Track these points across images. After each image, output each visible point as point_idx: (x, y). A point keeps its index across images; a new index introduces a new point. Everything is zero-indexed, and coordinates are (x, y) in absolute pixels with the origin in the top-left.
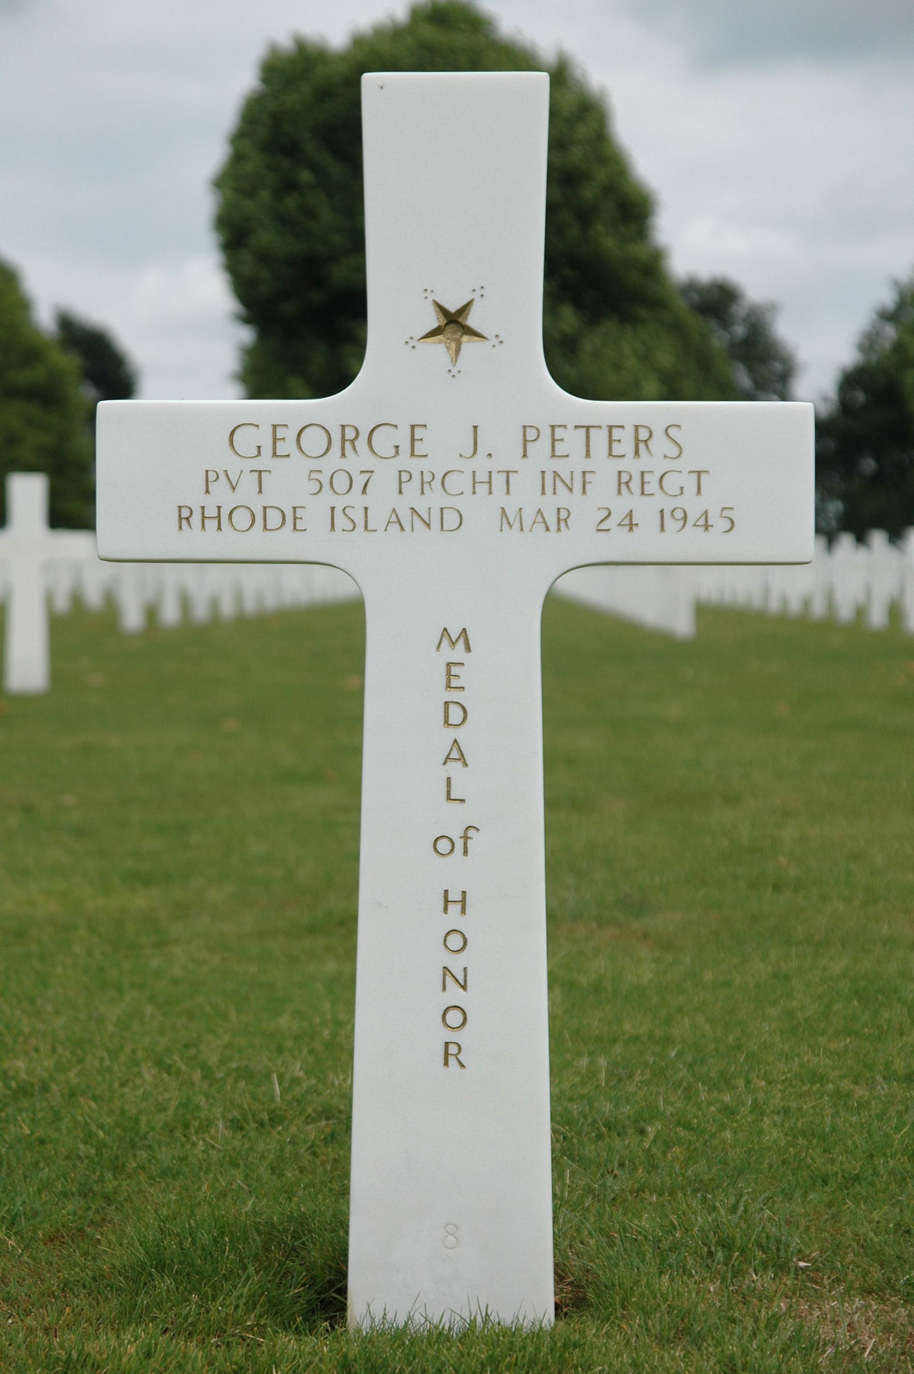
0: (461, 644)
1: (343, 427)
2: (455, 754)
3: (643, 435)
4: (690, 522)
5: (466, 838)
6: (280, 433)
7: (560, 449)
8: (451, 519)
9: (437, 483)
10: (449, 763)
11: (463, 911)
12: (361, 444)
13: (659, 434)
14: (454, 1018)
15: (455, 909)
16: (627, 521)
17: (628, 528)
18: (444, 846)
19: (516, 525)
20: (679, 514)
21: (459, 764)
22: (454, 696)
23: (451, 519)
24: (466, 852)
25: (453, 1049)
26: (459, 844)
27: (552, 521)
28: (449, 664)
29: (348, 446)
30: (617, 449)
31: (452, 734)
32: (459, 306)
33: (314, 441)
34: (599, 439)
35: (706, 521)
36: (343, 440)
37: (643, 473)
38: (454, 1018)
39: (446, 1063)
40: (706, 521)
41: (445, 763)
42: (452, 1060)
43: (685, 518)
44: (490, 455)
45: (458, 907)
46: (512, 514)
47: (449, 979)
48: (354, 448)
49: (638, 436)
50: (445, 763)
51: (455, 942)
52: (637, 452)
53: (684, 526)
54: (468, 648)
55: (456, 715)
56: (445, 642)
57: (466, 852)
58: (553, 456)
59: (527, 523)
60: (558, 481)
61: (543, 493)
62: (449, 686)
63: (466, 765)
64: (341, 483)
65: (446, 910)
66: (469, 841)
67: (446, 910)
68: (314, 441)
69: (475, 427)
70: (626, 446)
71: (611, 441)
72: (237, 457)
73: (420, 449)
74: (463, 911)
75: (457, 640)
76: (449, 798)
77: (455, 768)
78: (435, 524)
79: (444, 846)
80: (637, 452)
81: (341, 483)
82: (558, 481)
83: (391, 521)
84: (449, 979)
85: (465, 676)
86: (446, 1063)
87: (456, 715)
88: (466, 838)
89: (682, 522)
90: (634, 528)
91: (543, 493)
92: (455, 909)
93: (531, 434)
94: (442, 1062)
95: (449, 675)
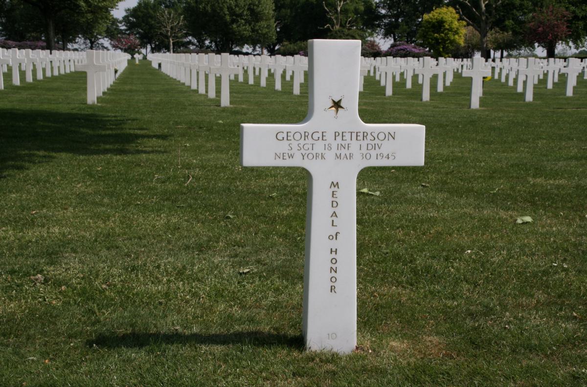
0: (337, 186)
1: (305, 132)
2: (334, 215)
3: (365, 134)
4: (384, 157)
5: (336, 235)
6: (289, 134)
7: (344, 138)
8: (368, 156)
9: (310, 136)
11: (336, 254)
12: (310, 136)
13: (369, 134)
18: (331, 237)
19: (339, 158)
21: (335, 217)
22: (334, 199)
23: (368, 156)
24: (336, 239)
25: (333, 288)
27: (348, 157)
28: (333, 192)
30: (359, 138)
34: (354, 135)
36: (305, 136)
37: (343, 133)
38: (333, 280)
39: (331, 291)
41: (331, 217)
42: (333, 291)
46: (338, 155)
47: (332, 270)
49: (45, 74)
51: (334, 261)
52: (363, 139)
54: (338, 188)
55: (335, 204)
56: (333, 186)
57: (336, 239)
59: (342, 158)
62: (333, 196)
65: (336, 249)
67: (336, 249)
68: (297, 136)
70: (361, 138)
71: (357, 136)
73: (324, 138)
74: (336, 254)
76: (333, 225)
77: (334, 218)
78: (281, 157)
79: (331, 237)
80: (363, 139)
84: (332, 270)
85: (337, 194)
86: (331, 291)
87: (335, 204)
88: (336, 235)
93: (337, 134)
94: (330, 291)
95: (333, 194)
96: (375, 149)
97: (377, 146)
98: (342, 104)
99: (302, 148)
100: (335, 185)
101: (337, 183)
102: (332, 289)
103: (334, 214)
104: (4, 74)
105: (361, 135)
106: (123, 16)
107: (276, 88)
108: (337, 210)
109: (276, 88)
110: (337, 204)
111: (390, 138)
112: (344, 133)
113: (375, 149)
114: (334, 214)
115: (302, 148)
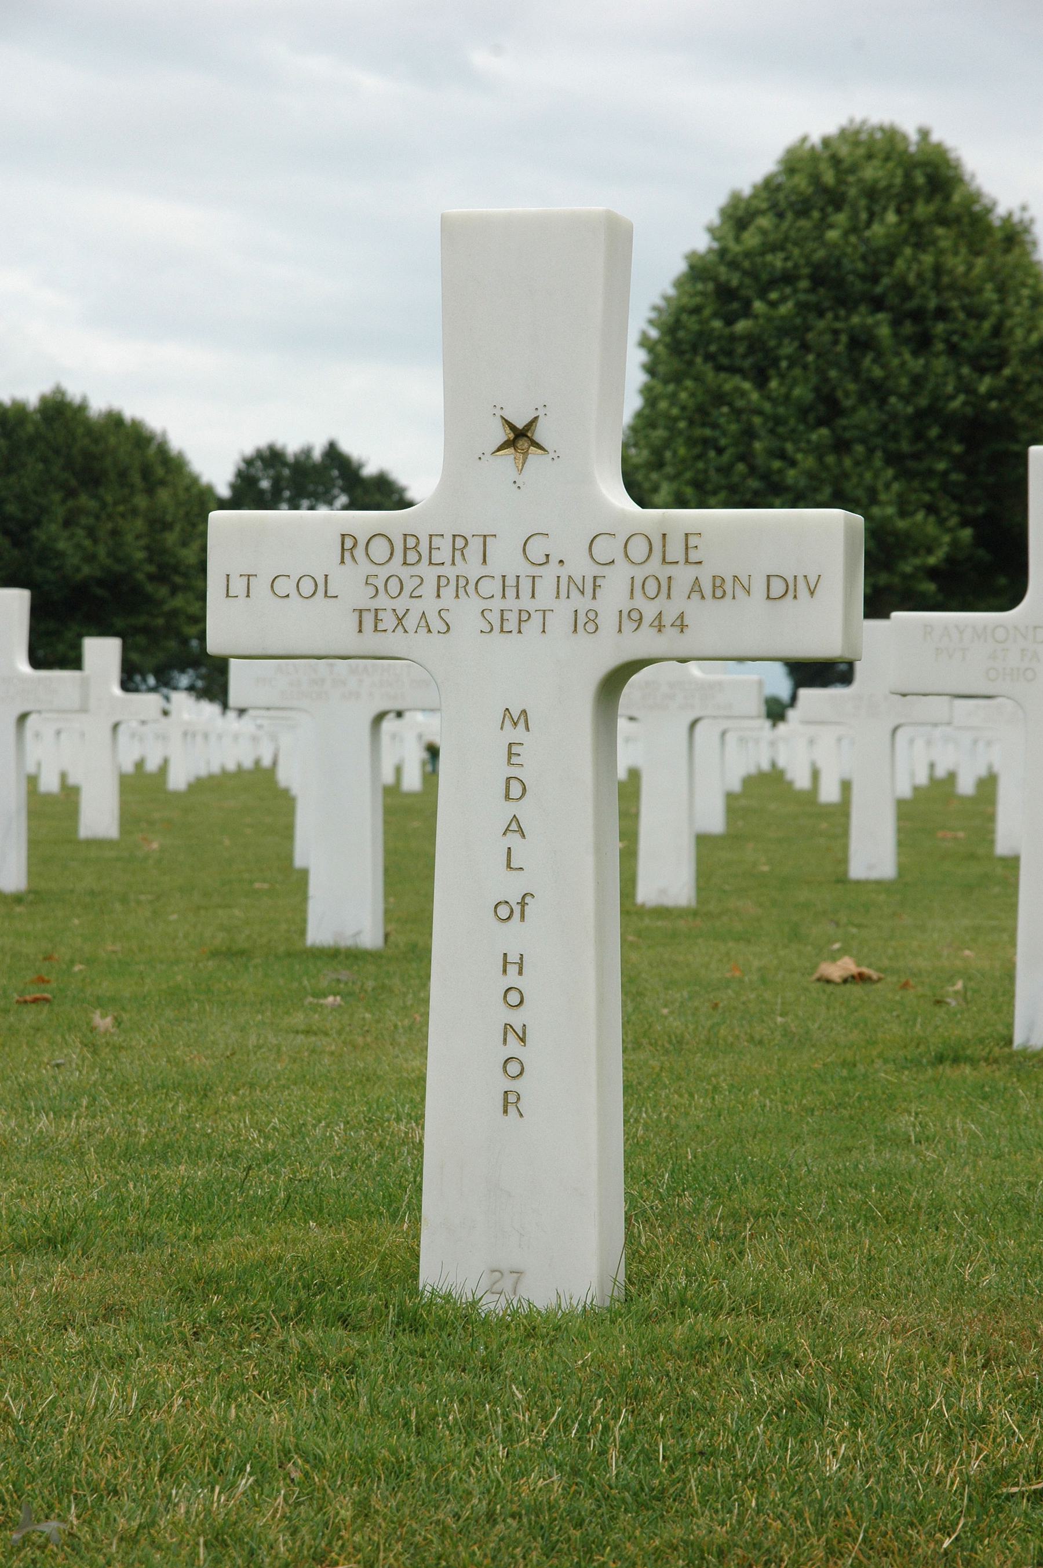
2: (514, 826)
5: (523, 904)
9: (471, 588)
10: (509, 834)
11: (520, 973)
12: (359, 552)
14: (513, 1068)
15: (512, 969)
16: (678, 623)
17: (656, 629)
20: (635, 615)
21: (518, 835)
25: (512, 1098)
26: (517, 910)
29: (458, 554)
31: (512, 808)
32: (508, 431)
33: (379, 550)
35: (660, 622)
37: (595, 578)
39: (505, 1112)
40: (660, 622)
42: (511, 1109)
43: (641, 619)
44: (561, 561)
45: (516, 968)
48: (353, 556)
50: (504, 834)
53: (639, 625)
54: (527, 729)
55: (516, 790)
58: (405, 563)
60: (572, 585)
61: (558, 597)
63: (523, 836)
64: (394, 586)
66: (526, 907)
67: (505, 971)
69: (664, 535)
72: (633, 565)
74: (520, 973)
75: (519, 718)
76: (509, 866)
77: (514, 839)
79: (504, 912)
81: (394, 586)
82: (572, 585)
83: (400, 617)
86: (505, 1112)
87: (516, 790)
89: (636, 625)
90: (662, 629)
91: (558, 597)
92: (512, 969)
94: (501, 1109)
95: (510, 754)
96: (669, 596)
97: (801, 581)
98: (540, 434)
99: (381, 589)
100: (521, 719)
101: (524, 712)
102: (509, 1102)
103: (515, 827)
104: (392, 793)
105: (446, 545)
106: (74, 392)
107: (858, 869)
108: (525, 810)
109: (858, 869)
110: (524, 789)
111: (739, 591)
112: (598, 580)
113: (669, 596)
114: (515, 827)
115: (381, 589)
